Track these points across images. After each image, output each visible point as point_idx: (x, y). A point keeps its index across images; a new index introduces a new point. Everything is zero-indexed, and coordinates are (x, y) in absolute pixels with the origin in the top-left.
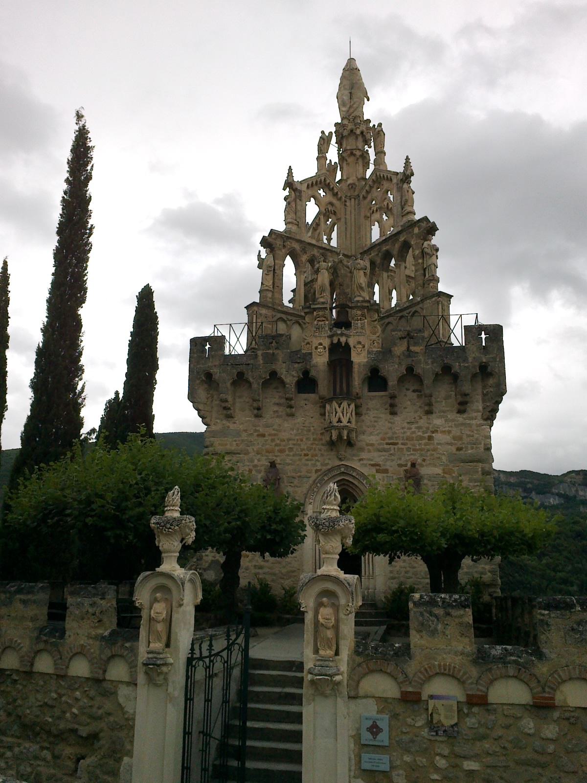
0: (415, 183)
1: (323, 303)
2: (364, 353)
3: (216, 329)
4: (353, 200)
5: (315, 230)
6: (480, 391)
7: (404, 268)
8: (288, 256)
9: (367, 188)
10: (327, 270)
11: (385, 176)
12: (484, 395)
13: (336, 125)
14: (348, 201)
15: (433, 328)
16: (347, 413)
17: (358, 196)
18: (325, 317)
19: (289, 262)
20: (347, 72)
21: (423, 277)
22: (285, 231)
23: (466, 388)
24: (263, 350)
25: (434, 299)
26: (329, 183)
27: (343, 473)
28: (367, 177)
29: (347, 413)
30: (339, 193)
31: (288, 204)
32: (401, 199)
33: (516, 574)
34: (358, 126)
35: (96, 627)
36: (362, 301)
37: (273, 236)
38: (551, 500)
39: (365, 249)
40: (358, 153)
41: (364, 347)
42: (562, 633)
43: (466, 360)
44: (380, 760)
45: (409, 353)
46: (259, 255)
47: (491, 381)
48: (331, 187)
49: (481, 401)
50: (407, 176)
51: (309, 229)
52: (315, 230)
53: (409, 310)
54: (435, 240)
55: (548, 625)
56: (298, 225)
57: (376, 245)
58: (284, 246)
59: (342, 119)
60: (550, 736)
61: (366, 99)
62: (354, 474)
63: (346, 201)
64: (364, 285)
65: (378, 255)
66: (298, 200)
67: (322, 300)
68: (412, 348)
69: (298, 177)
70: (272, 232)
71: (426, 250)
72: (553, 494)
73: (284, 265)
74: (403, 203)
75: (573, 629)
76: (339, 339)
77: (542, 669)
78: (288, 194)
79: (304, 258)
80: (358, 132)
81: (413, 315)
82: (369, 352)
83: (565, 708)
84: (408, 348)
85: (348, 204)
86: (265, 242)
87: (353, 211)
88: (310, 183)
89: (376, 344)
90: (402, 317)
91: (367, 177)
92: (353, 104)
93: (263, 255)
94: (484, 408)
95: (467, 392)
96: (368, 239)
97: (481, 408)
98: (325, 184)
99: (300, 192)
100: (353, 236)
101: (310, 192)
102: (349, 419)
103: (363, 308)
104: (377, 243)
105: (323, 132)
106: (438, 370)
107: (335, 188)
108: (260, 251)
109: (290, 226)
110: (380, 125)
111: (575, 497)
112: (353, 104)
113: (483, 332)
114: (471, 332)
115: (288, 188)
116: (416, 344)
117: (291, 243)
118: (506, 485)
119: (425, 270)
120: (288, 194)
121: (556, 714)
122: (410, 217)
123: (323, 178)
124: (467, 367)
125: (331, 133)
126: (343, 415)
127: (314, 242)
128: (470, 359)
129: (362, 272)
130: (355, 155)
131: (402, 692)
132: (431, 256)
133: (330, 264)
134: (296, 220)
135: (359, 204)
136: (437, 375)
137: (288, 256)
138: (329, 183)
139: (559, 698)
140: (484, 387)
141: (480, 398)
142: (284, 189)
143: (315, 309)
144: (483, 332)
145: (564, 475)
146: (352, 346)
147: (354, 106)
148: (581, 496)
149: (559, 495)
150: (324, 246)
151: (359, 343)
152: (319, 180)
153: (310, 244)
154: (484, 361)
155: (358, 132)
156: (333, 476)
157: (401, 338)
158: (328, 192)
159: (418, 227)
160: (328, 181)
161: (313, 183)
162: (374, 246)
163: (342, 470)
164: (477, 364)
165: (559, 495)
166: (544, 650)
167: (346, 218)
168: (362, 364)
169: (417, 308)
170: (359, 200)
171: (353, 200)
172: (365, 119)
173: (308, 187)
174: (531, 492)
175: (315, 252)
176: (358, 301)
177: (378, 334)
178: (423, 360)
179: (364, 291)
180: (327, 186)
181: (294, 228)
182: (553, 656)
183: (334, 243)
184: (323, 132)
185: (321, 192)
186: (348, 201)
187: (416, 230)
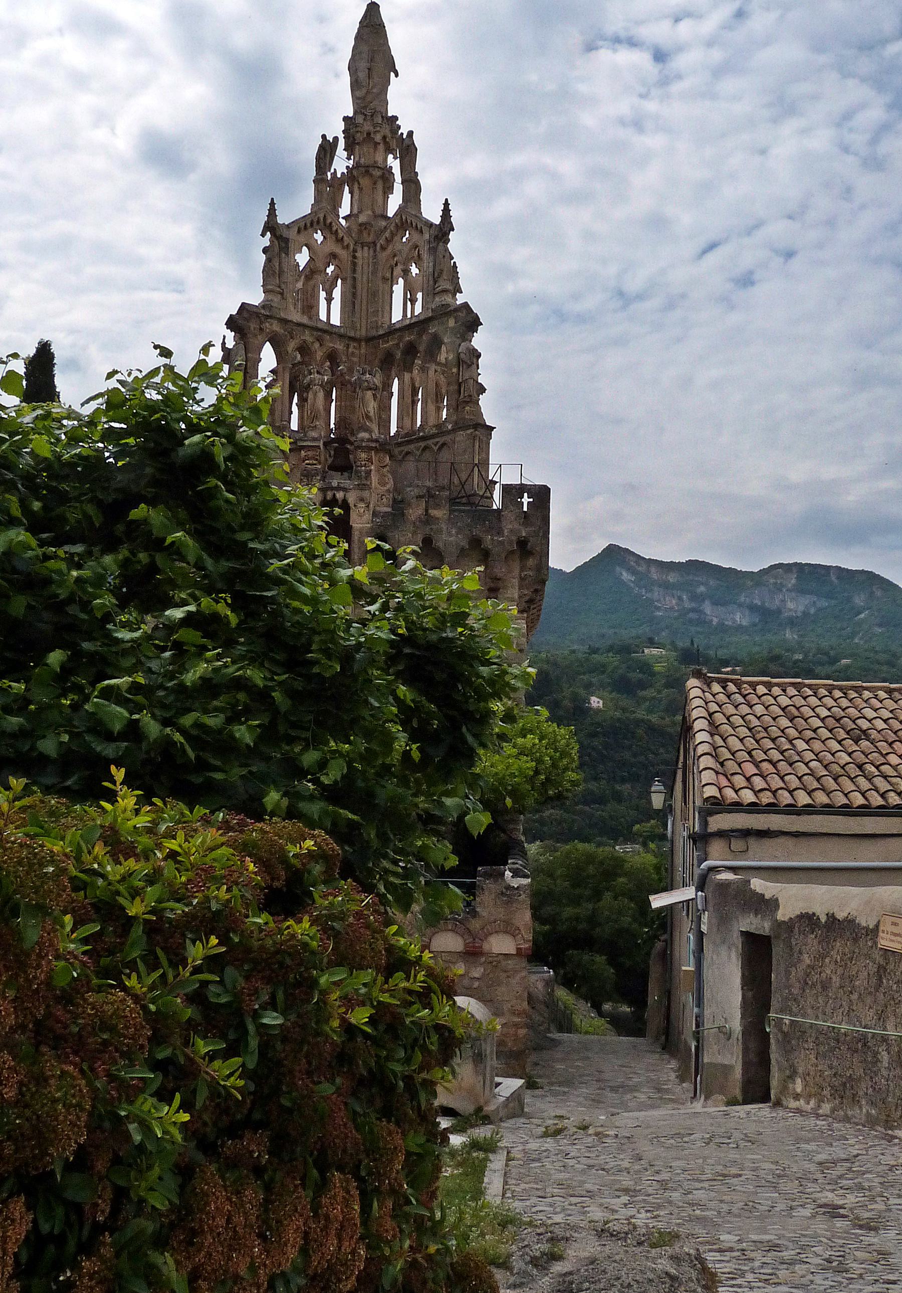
0: (455, 244)
1: (314, 439)
2: (368, 516)
4: (366, 248)
5: (308, 278)
6: (516, 572)
9: (387, 234)
10: (321, 386)
11: (414, 224)
12: (522, 579)
14: (359, 249)
15: (464, 478)
17: (374, 244)
18: (317, 460)
20: (366, 30)
21: (457, 396)
22: (264, 306)
23: (500, 570)
25: (469, 432)
26: (331, 223)
28: (390, 214)
30: (345, 238)
31: (269, 261)
32: (434, 266)
33: (661, 750)
34: (378, 129)
36: (369, 440)
37: (245, 315)
38: (738, 617)
39: (381, 332)
40: (377, 173)
41: (368, 506)
42: (493, 896)
43: (500, 533)
45: (428, 519)
47: (531, 562)
48: (334, 229)
49: (517, 588)
50: (446, 226)
51: (300, 277)
52: (308, 278)
53: (437, 440)
54: (478, 341)
55: (483, 889)
56: (282, 294)
57: (396, 330)
58: (261, 329)
59: (355, 113)
60: (477, 976)
61: (392, 74)
63: (355, 251)
64: (372, 414)
65: (398, 344)
66: (284, 255)
67: (314, 434)
68: (434, 512)
69: (283, 218)
70: (244, 307)
71: (462, 356)
72: (740, 605)
74: (436, 275)
75: (502, 893)
76: (334, 495)
77: (475, 924)
78: (268, 244)
79: (291, 346)
80: (378, 138)
81: (440, 449)
82: (375, 514)
83: (488, 954)
84: (427, 511)
85: (358, 254)
86: (231, 323)
87: (365, 268)
88: (302, 224)
89: (385, 500)
90: (425, 448)
91: (390, 214)
92: (372, 88)
93: (230, 344)
94: (520, 597)
95: (500, 575)
96: (387, 319)
97: (516, 596)
98: (325, 225)
99: (286, 241)
100: (364, 307)
101: (302, 238)
103: (370, 449)
104: (397, 326)
105: (324, 137)
106: (464, 544)
107: (339, 231)
108: (224, 337)
109: (270, 297)
110: (411, 134)
111: (779, 611)
112: (372, 88)
113: (526, 495)
114: (512, 492)
115: (268, 233)
116: (437, 506)
117: (271, 325)
118: (660, 586)
119: (460, 385)
121: (483, 959)
122: (448, 299)
123: (321, 216)
124: (502, 543)
125: (336, 139)
127: (305, 320)
128: (506, 533)
129: (369, 394)
130: (371, 175)
131: (517, 949)
132: (469, 366)
133: (326, 378)
134: (279, 287)
135: (375, 257)
136: (463, 550)
137: (268, 343)
138: (331, 223)
139: (486, 947)
140: (522, 569)
141: (516, 581)
142: (263, 235)
143: (303, 447)
144: (526, 495)
145: (764, 572)
146: (352, 505)
147: (375, 90)
148: (791, 610)
149: (752, 608)
150: (320, 326)
151: (362, 500)
152: (315, 220)
153: (299, 325)
154: (524, 534)
155: (378, 138)
157: (419, 497)
158: (328, 236)
159: (455, 318)
160: (329, 221)
161: (306, 225)
162: (394, 331)
164: (514, 538)
165: (752, 608)
166: (478, 910)
167: (354, 278)
168: (364, 531)
169: (447, 438)
170: (375, 251)
171: (366, 248)
172: (390, 114)
173: (299, 231)
174: (703, 600)
175: (308, 337)
176: (362, 440)
177: (388, 486)
178: (445, 528)
179: (371, 421)
180: (329, 228)
181: (276, 299)
182: (484, 914)
183: (336, 320)
184: (324, 137)
185: (319, 237)
186: (359, 249)
187: (451, 323)
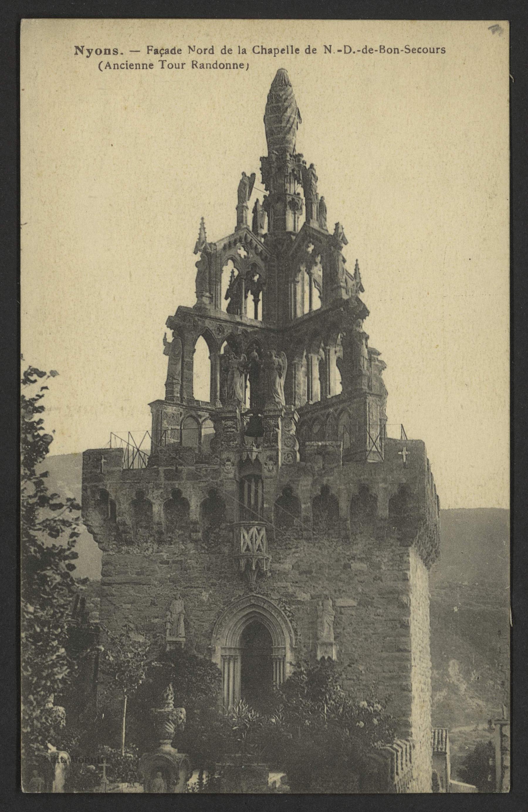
3: (113, 436)
7: (334, 352)
8: (201, 337)
13: (262, 159)
16: (256, 540)
19: (201, 345)
24: (166, 466)
27: (253, 604)
29: (256, 540)
35: (156, 571)
44: (414, 659)
46: (165, 339)
62: (265, 606)
73: (194, 351)
93: (170, 339)
102: (259, 546)
105: (244, 174)
107: (259, 246)
120: (200, 259)
125: (253, 175)
126: (252, 543)
137: (201, 337)
156: (244, 608)
163: (253, 601)
172: (264, 185)
184: (244, 174)
